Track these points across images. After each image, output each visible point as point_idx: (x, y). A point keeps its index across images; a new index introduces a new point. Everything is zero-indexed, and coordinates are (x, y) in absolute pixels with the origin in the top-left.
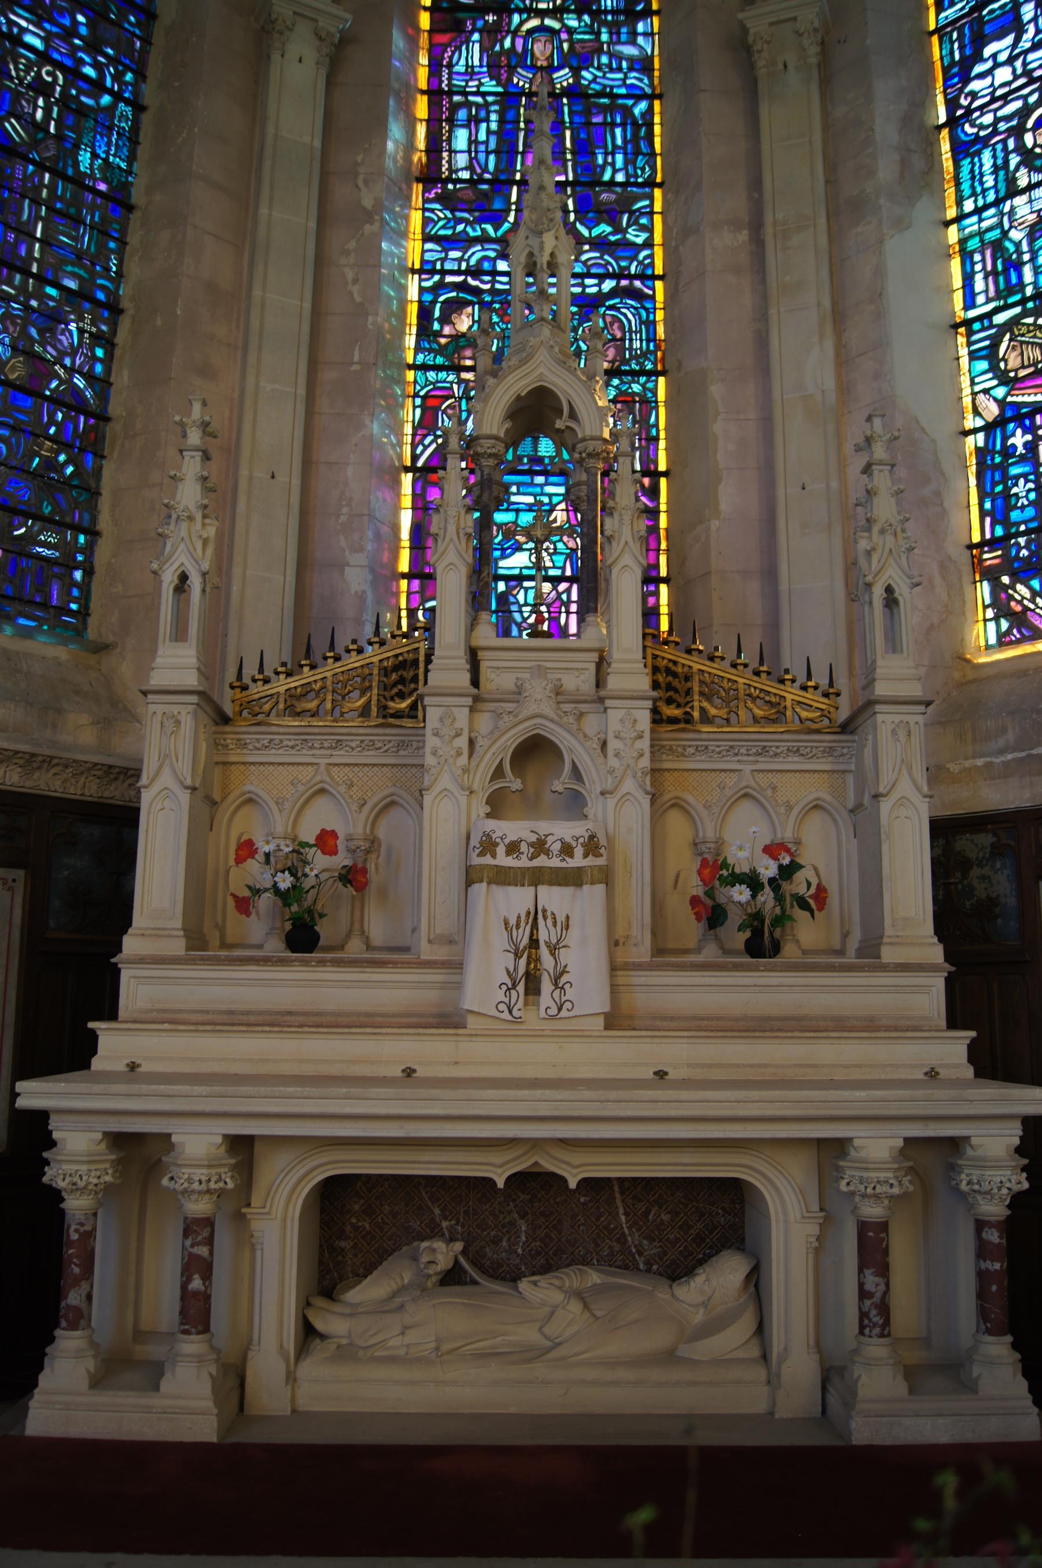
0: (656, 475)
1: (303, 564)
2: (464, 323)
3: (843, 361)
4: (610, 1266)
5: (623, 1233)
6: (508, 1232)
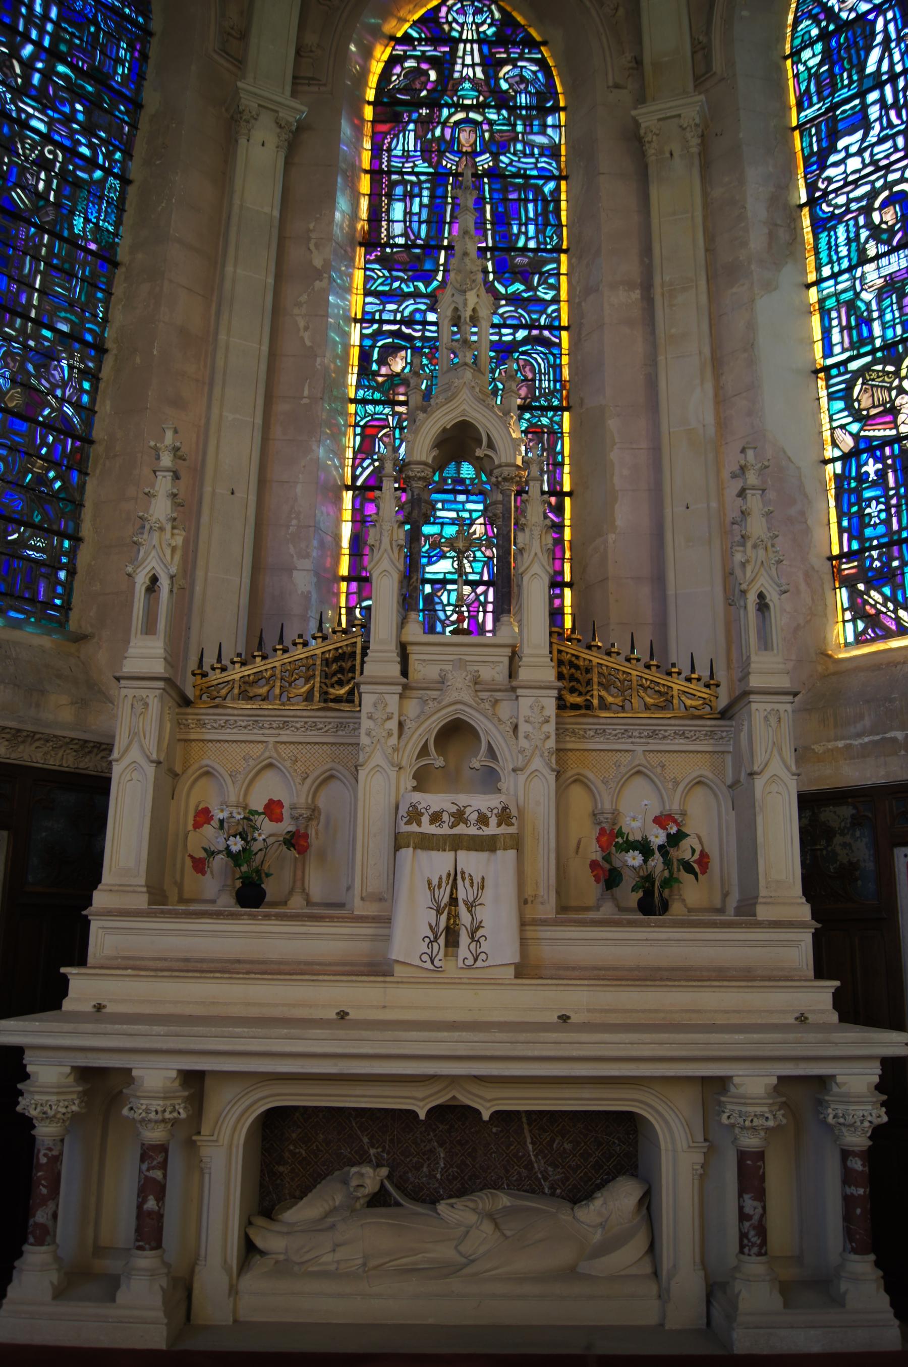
2: (398, 365)
3: (721, 400)
4: (519, 1190)
5: (531, 1160)
6: (428, 1159)
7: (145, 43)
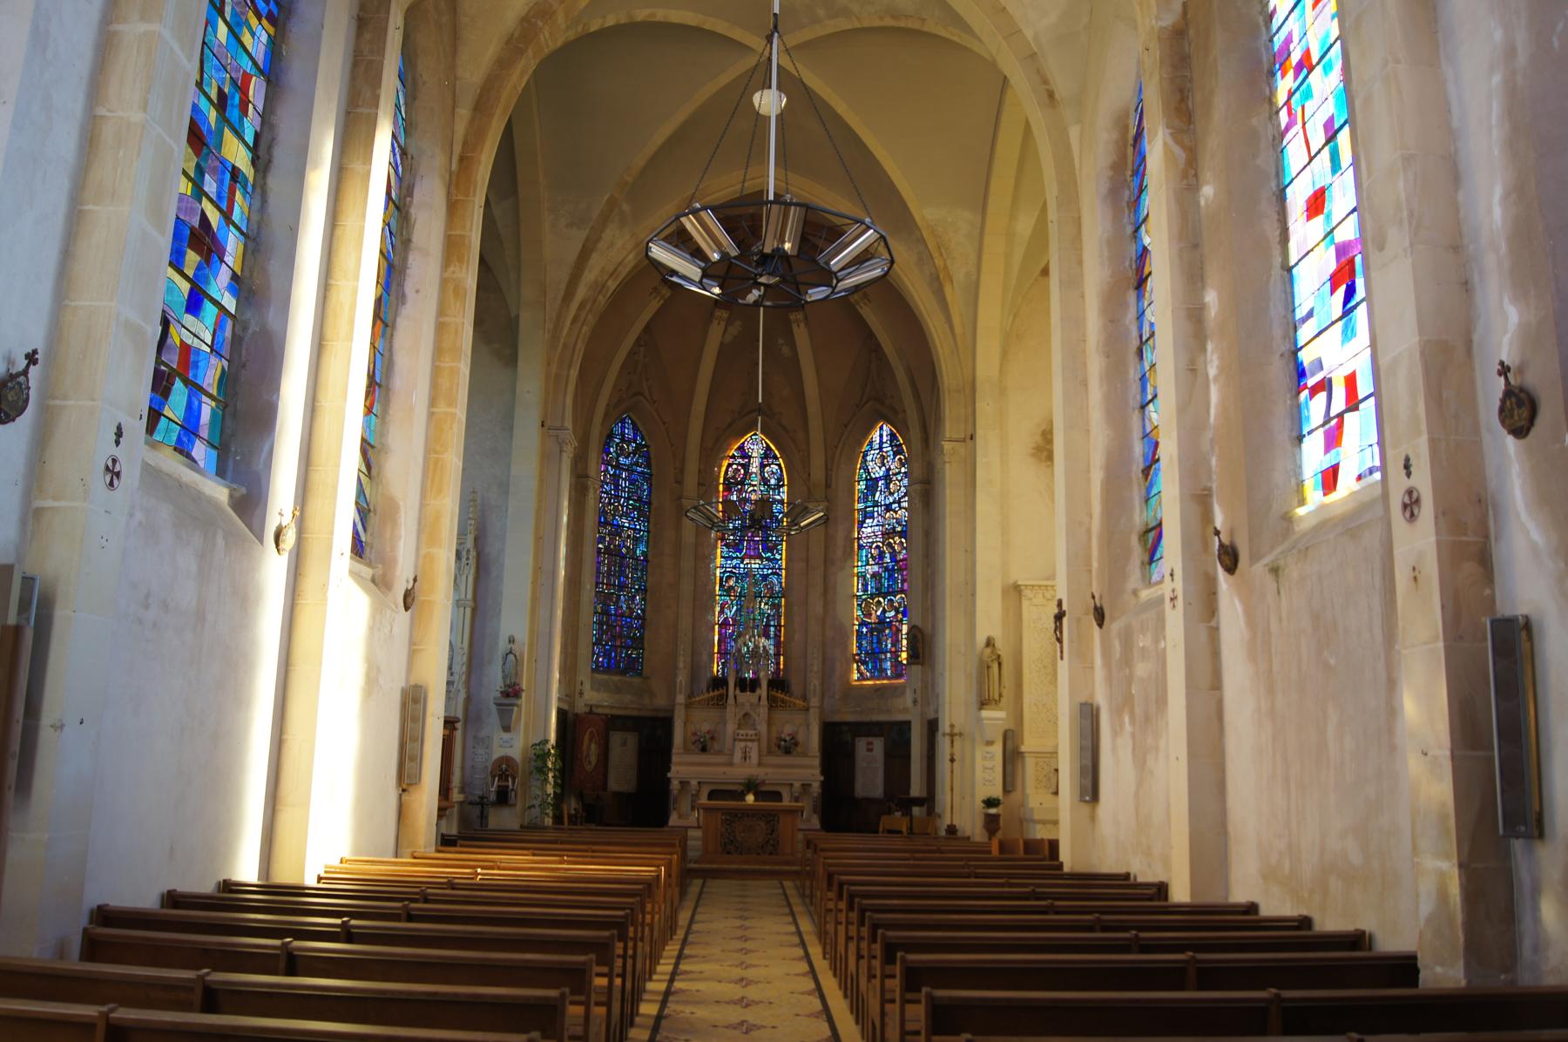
2: (731, 583)
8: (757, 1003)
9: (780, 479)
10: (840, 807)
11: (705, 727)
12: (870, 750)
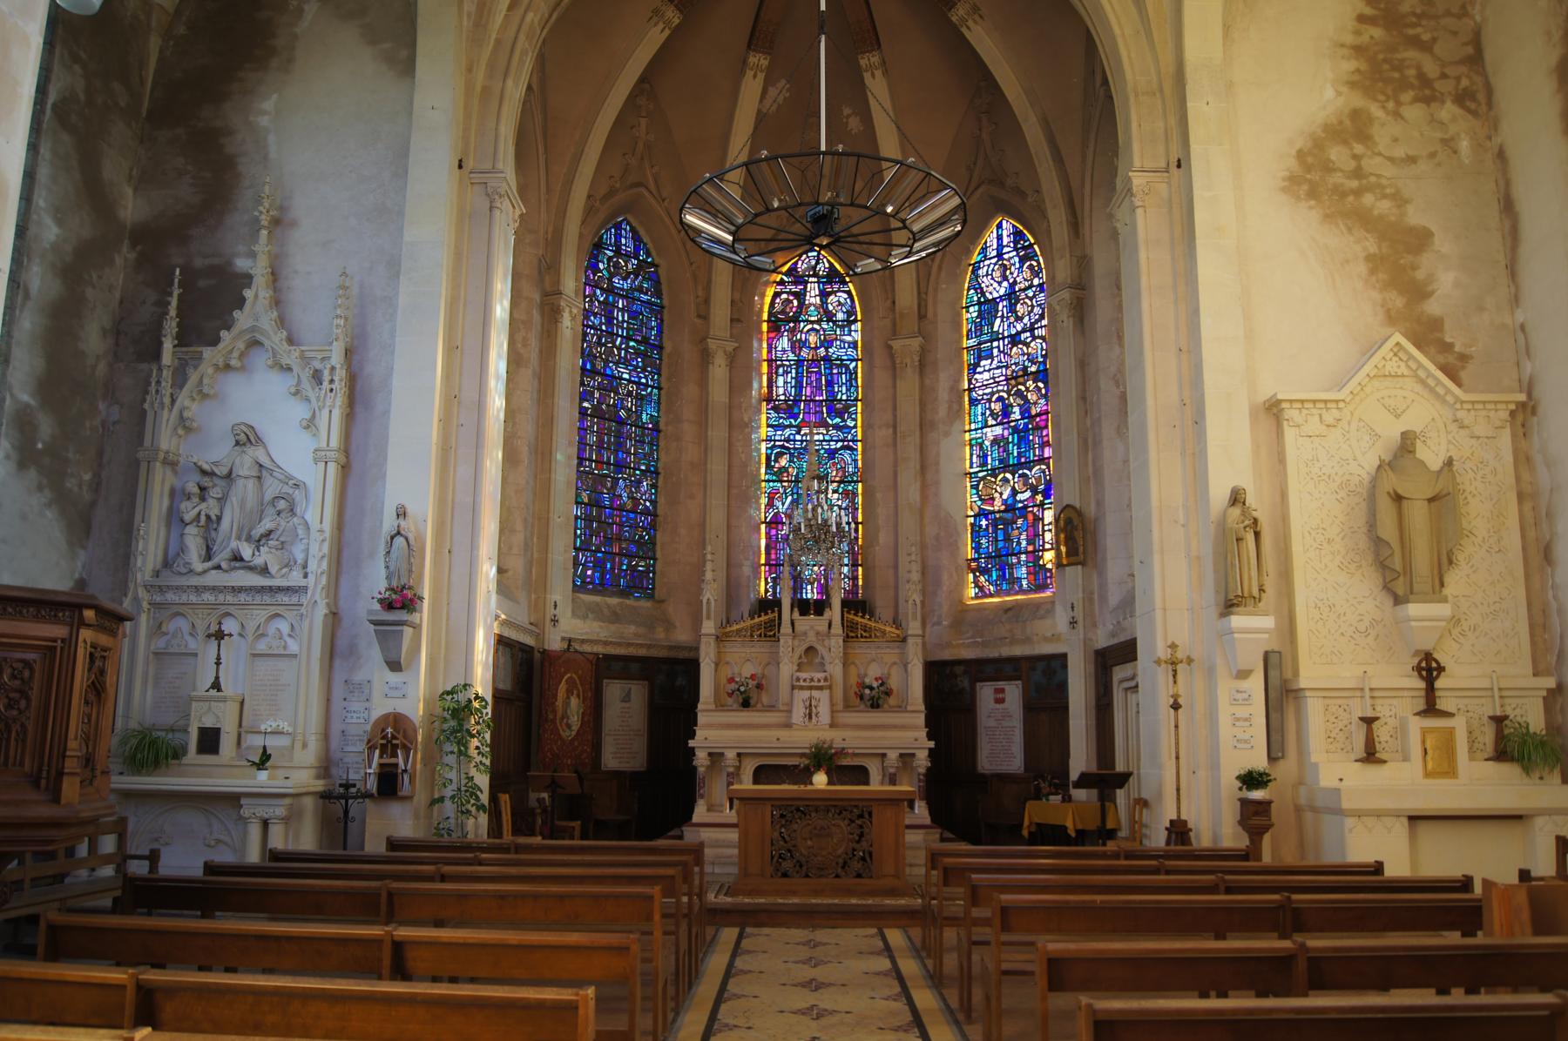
0: (857, 523)
1: (728, 565)
2: (783, 462)
3: (924, 487)
7: (661, 312)
8: (830, 985)
9: (851, 312)
10: (961, 794)
11: (748, 670)
12: (1000, 701)
